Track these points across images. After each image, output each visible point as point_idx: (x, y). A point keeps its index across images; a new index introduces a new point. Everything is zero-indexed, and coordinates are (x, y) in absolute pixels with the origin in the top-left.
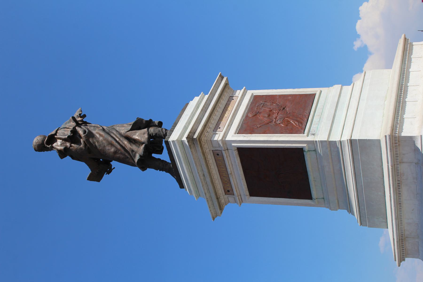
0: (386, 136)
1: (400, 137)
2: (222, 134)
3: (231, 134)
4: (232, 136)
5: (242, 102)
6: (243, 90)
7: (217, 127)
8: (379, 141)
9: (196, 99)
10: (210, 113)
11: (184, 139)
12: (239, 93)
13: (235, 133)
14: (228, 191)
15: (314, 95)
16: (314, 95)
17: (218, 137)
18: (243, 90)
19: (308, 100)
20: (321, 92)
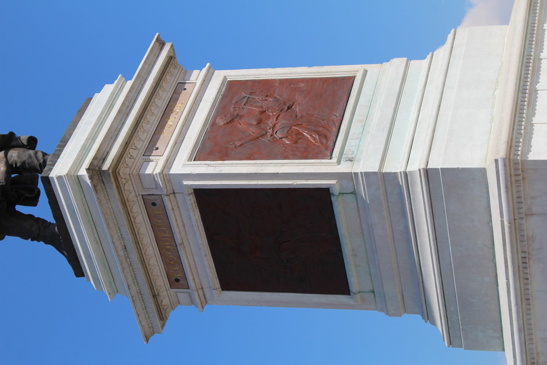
0: (496, 161)
1: (525, 162)
2: (162, 161)
3: (181, 160)
4: (177, 169)
5: (204, 93)
6: (204, 70)
7: (151, 147)
8: (483, 172)
9: (108, 89)
10: (136, 118)
11: (83, 172)
12: (197, 77)
13: (190, 159)
14: (177, 280)
15: (351, 80)
16: (351, 80)
17: (154, 167)
18: (204, 70)
19: (349, 81)
20: (365, 72)
